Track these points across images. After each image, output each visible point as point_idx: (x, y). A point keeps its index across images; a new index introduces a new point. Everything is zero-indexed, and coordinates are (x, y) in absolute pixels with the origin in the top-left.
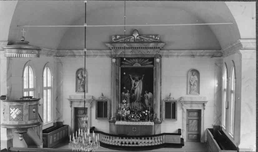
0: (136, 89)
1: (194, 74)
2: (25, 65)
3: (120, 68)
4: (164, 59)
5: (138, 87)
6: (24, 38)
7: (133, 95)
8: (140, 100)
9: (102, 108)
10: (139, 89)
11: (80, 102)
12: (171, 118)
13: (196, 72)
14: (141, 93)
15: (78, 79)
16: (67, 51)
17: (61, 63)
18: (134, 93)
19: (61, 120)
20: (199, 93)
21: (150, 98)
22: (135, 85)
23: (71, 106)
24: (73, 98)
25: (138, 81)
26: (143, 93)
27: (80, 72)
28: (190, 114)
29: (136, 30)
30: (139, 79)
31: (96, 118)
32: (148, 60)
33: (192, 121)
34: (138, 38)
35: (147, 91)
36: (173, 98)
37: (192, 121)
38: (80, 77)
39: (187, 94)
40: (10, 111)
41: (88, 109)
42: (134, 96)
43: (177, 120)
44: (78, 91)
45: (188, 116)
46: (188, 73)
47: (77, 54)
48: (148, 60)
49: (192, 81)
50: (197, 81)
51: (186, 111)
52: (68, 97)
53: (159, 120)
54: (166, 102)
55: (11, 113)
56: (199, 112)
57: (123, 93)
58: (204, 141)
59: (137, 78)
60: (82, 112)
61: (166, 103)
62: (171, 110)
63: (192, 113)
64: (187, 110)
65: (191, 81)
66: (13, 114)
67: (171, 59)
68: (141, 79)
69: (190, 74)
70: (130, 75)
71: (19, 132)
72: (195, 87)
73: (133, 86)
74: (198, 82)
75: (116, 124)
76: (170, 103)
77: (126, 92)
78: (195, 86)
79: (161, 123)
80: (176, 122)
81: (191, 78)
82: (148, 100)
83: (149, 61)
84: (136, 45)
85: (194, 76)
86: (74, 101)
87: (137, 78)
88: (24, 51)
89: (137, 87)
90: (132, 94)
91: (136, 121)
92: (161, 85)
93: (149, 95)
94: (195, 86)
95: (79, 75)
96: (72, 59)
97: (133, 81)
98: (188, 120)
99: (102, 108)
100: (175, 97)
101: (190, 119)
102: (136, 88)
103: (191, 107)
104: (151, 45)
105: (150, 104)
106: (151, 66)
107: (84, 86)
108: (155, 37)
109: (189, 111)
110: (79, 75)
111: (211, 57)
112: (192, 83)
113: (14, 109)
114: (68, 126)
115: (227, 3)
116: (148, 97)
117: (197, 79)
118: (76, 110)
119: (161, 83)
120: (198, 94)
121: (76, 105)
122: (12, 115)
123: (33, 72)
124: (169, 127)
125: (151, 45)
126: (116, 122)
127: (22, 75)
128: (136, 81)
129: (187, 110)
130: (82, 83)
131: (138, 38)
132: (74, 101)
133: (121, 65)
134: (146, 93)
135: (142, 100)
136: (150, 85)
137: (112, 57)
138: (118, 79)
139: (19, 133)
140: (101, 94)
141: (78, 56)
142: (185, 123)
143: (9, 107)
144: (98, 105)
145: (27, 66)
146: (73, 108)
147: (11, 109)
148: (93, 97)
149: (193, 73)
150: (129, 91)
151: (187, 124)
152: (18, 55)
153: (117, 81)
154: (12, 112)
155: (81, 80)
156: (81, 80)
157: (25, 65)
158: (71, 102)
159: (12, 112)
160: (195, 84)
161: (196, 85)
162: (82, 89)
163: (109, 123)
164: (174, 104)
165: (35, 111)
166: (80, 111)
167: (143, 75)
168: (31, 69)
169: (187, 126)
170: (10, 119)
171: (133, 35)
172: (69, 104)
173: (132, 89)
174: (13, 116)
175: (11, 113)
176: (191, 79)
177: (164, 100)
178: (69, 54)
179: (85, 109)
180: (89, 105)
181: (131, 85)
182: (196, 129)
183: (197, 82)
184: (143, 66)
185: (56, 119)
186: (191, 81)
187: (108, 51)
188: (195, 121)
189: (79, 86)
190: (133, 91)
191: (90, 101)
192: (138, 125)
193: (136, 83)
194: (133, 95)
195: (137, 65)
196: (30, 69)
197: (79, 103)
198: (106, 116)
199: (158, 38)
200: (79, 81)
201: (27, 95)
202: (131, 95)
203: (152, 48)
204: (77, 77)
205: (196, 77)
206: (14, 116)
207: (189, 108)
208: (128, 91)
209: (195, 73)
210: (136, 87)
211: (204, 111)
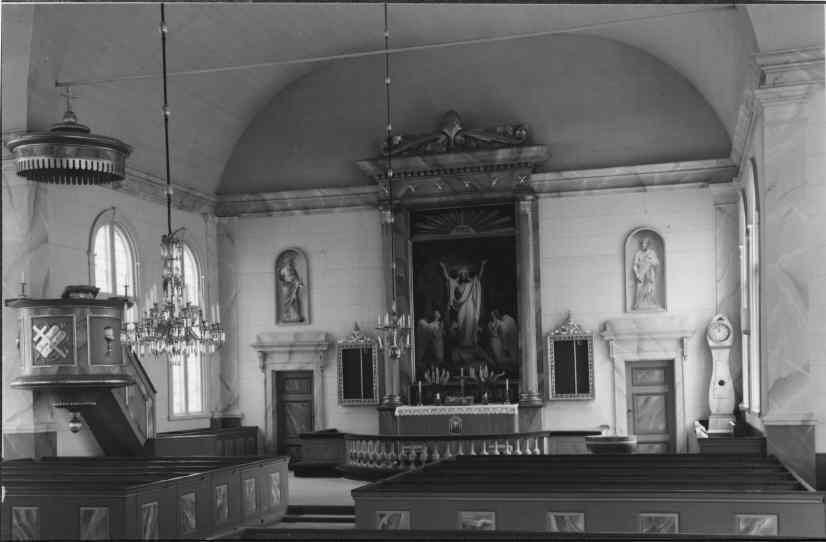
0: (463, 307)
1: (645, 245)
2: (96, 220)
3: (410, 243)
4: (547, 204)
5: (470, 303)
6: (75, 117)
7: (455, 325)
8: (476, 339)
9: (357, 371)
10: (470, 304)
11: (291, 352)
12: (574, 392)
13: (651, 238)
14: (477, 318)
15: (282, 282)
16: (246, 197)
17: (228, 235)
18: (457, 320)
19: (236, 413)
20: (664, 306)
21: (508, 335)
22: (458, 294)
23: (264, 368)
24: (267, 340)
25: (467, 281)
26: (485, 319)
27: (286, 260)
28: (639, 376)
29: (451, 113)
30: (472, 275)
31: (340, 402)
32: (497, 212)
33: (646, 401)
34: (459, 137)
35: (497, 311)
36: (579, 326)
37: (646, 401)
38: (288, 279)
39: (625, 310)
40: (34, 334)
41: (315, 373)
42: (456, 329)
43: (593, 396)
44: (285, 322)
45: (633, 382)
46: (626, 240)
47: (276, 206)
48: (497, 212)
49: (638, 267)
50: (655, 268)
51: (622, 366)
52: (254, 341)
53: (536, 398)
54: (557, 340)
55: (35, 339)
56: (668, 367)
57: (423, 322)
58: (670, 443)
59: (464, 271)
60: (296, 385)
61: (556, 343)
62: (572, 367)
63: (644, 373)
64: (628, 363)
65: (636, 268)
66: (42, 343)
67: (567, 201)
68: (478, 273)
69: (632, 244)
70: (442, 265)
71: (67, 404)
72: (652, 287)
73: (452, 297)
74: (661, 270)
75: (397, 413)
76: (572, 342)
77: (431, 319)
78: (652, 282)
79: (540, 407)
80: (592, 404)
81: (635, 256)
82: (502, 341)
83: (502, 215)
84: (452, 159)
85: (645, 250)
86: (273, 352)
87: (464, 271)
88: (69, 149)
89: (467, 299)
90: (451, 323)
91: (460, 404)
92: (538, 287)
93: (506, 323)
94: (652, 282)
95: (285, 271)
96: (264, 220)
97: (453, 283)
98: (633, 398)
99: (357, 371)
100: (586, 322)
101: (639, 395)
102: (461, 304)
103: (639, 350)
104: (502, 155)
105: (507, 354)
106: (504, 232)
107: (297, 304)
108: (514, 131)
109: (635, 368)
110: (285, 271)
111: (703, 187)
112: (640, 276)
113: (45, 328)
114: (257, 428)
115: (751, 8)
116: (499, 330)
117: (655, 261)
118: (281, 379)
119: (537, 280)
120: (660, 309)
121: (279, 363)
122: (38, 348)
123: (128, 249)
124: (562, 417)
125: (502, 155)
126: (398, 409)
127: (87, 248)
128: (460, 282)
129: (628, 363)
130: (294, 296)
131: (459, 137)
132: (273, 352)
133: (412, 235)
134: (495, 319)
135: (484, 338)
136: (506, 287)
137: (378, 204)
138: (402, 275)
139: (66, 407)
140: (352, 327)
141: (278, 211)
142: (622, 405)
143: (30, 322)
144: (344, 361)
145: (104, 224)
146: (269, 373)
147: (35, 328)
148: (327, 335)
149: (641, 243)
150: (441, 313)
151: (629, 411)
152: (58, 160)
153: (400, 282)
154: (40, 339)
155: (291, 285)
156: (291, 285)
157: (96, 220)
158: (264, 356)
159: (40, 339)
160: (648, 277)
161: (653, 280)
162: (294, 316)
163: (377, 412)
164: (584, 347)
165: (112, 338)
166: (291, 381)
167: (484, 263)
168: (121, 245)
169: (628, 417)
170: (34, 359)
171: (445, 130)
172: (258, 362)
173: (449, 308)
174: (43, 348)
175: (35, 339)
176: (637, 261)
177: (548, 334)
178: (253, 207)
179: (306, 377)
180: (317, 363)
181: (446, 298)
182: (661, 427)
183: (655, 270)
184: (485, 234)
185: (219, 409)
186: (636, 268)
187: (368, 189)
188: (655, 398)
189: (286, 305)
190: (454, 314)
191: (320, 348)
192: (467, 413)
193: (461, 290)
194: (455, 325)
195: (464, 231)
196: (116, 237)
197: (287, 356)
198: (369, 394)
199: (524, 132)
200: (285, 290)
201: (181, 409)
202: (446, 328)
203: (506, 166)
204: (280, 278)
205: (652, 254)
206: (45, 350)
207: (634, 357)
208: (438, 314)
209: (649, 243)
210: (462, 299)
211: (685, 364)
